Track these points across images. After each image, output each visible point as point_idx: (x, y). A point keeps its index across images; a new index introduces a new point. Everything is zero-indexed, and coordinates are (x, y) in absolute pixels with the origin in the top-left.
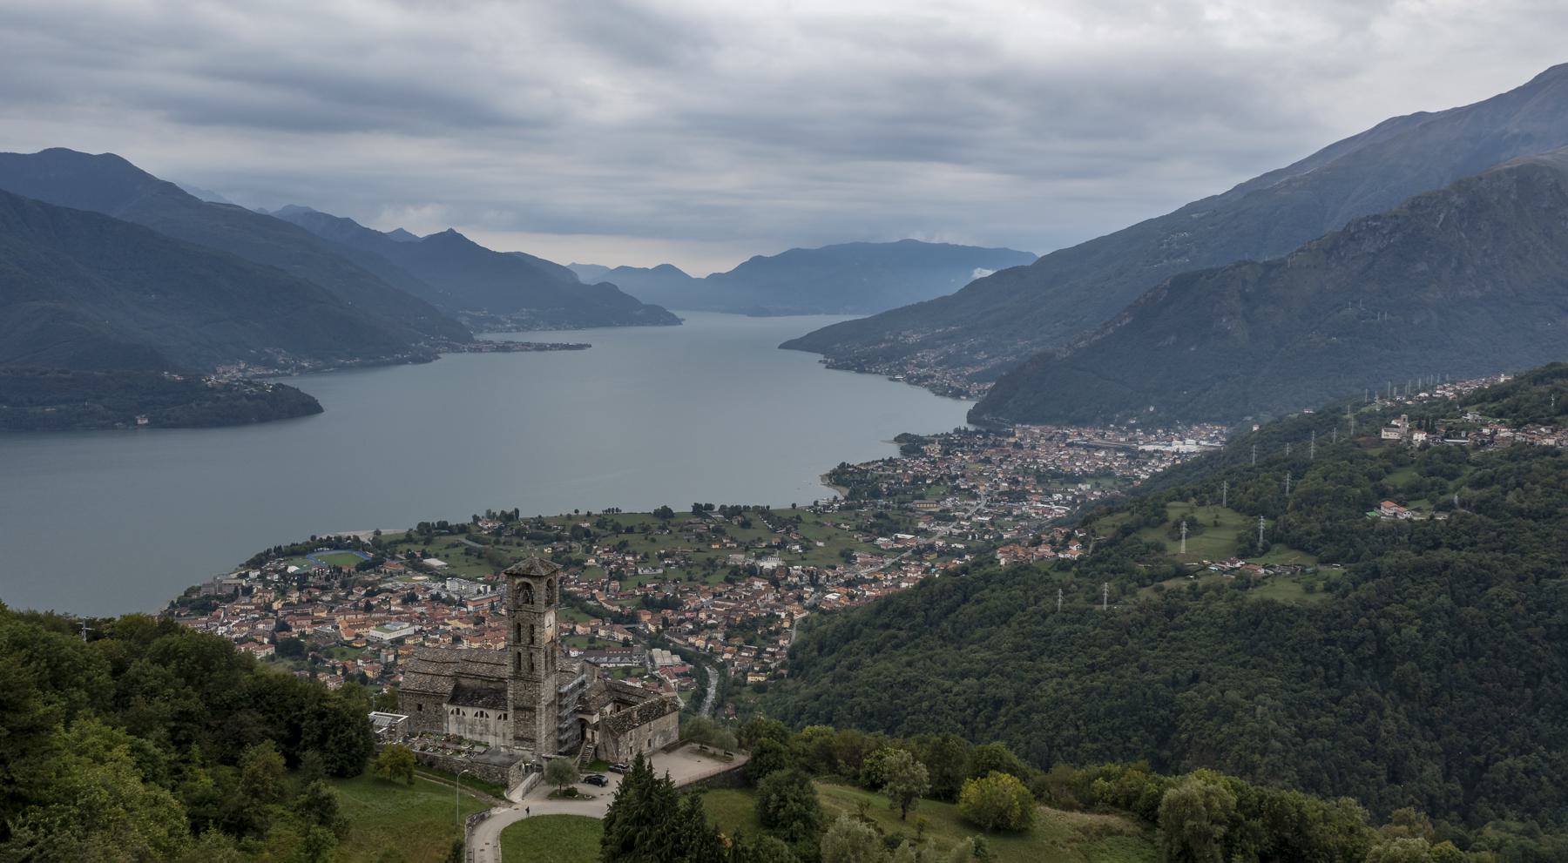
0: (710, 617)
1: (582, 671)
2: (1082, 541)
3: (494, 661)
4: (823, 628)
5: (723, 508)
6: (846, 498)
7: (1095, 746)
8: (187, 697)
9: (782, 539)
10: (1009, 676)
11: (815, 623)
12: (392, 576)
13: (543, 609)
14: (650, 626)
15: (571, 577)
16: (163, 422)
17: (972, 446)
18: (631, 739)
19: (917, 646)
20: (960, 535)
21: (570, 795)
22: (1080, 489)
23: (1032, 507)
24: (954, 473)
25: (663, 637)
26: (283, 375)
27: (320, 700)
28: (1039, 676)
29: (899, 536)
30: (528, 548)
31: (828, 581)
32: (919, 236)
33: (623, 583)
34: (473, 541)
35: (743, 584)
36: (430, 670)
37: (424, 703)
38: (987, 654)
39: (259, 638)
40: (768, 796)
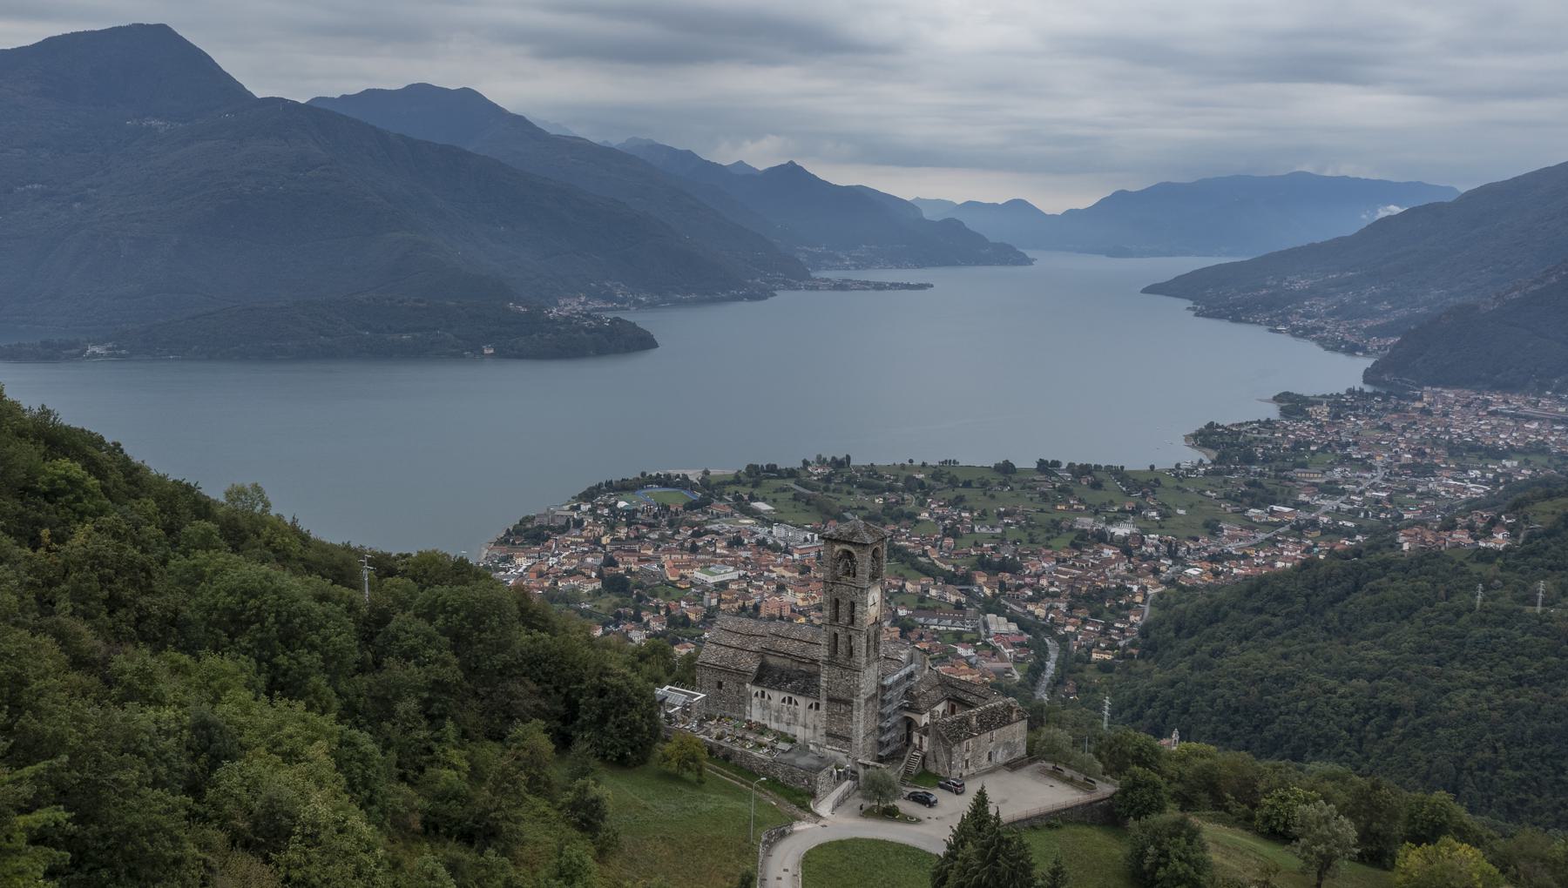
0: (1052, 584)
1: (911, 661)
2: (1510, 528)
3: (807, 639)
4: (1182, 606)
5: (1071, 465)
6: (1214, 462)
7: (1517, 774)
8: (445, 664)
9: (1137, 504)
10: (1409, 680)
11: (1173, 600)
12: (718, 517)
13: (866, 585)
14: (985, 589)
15: (903, 530)
16: (507, 353)
17: (1369, 410)
18: (967, 750)
19: (1294, 637)
20: (1349, 511)
21: (890, 814)
22: (1504, 466)
23: (1443, 484)
24: (1344, 439)
25: (999, 602)
26: (622, 309)
27: (601, 674)
28: (1449, 685)
29: (1275, 508)
30: (859, 497)
31: (1189, 553)
32: (1308, 168)
33: (958, 541)
34: (802, 486)
35: (1091, 551)
36: (733, 643)
37: (727, 681)
38: (1383, 653)
39: (587, 572)
40: (1144, 848)
